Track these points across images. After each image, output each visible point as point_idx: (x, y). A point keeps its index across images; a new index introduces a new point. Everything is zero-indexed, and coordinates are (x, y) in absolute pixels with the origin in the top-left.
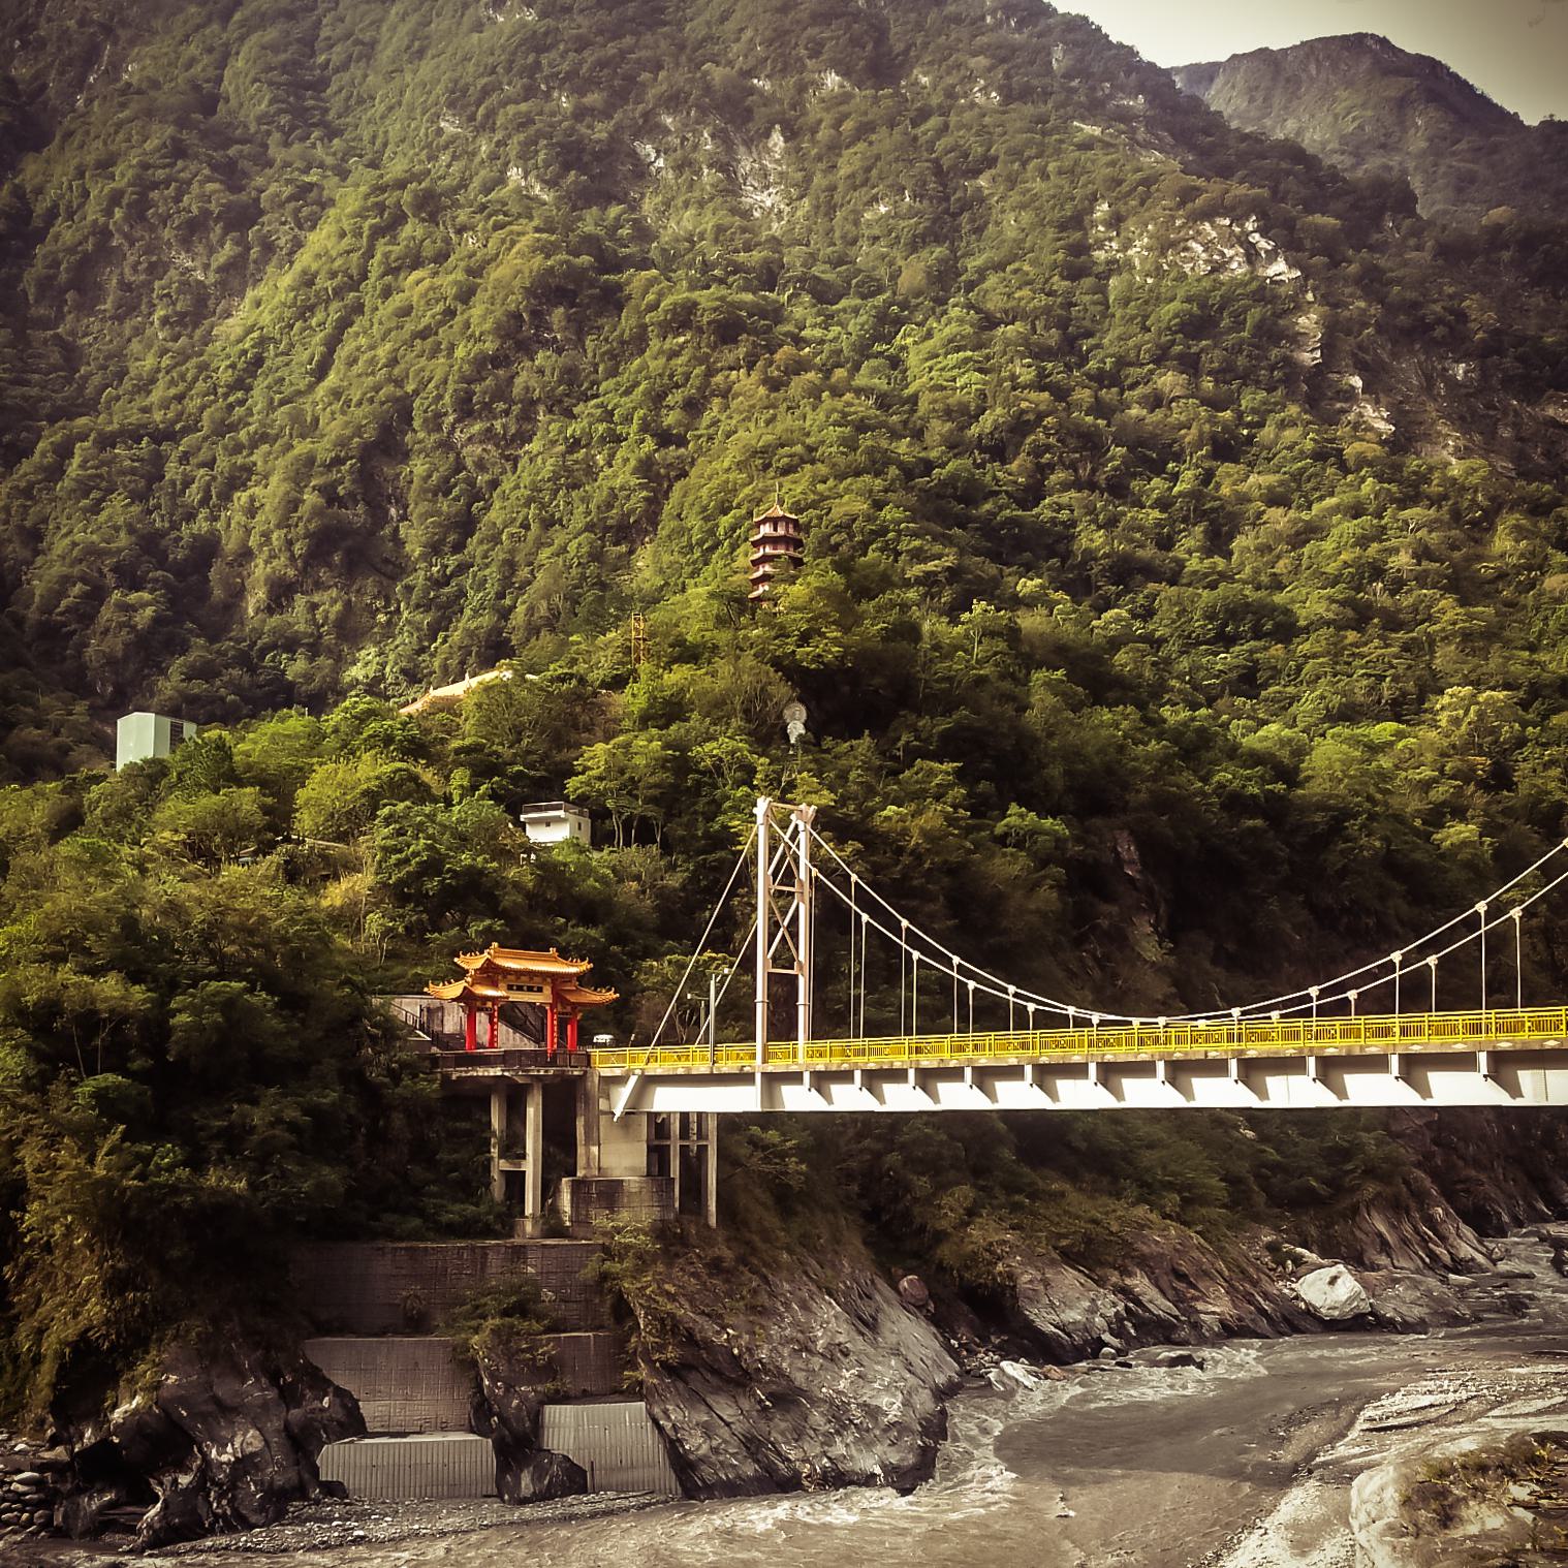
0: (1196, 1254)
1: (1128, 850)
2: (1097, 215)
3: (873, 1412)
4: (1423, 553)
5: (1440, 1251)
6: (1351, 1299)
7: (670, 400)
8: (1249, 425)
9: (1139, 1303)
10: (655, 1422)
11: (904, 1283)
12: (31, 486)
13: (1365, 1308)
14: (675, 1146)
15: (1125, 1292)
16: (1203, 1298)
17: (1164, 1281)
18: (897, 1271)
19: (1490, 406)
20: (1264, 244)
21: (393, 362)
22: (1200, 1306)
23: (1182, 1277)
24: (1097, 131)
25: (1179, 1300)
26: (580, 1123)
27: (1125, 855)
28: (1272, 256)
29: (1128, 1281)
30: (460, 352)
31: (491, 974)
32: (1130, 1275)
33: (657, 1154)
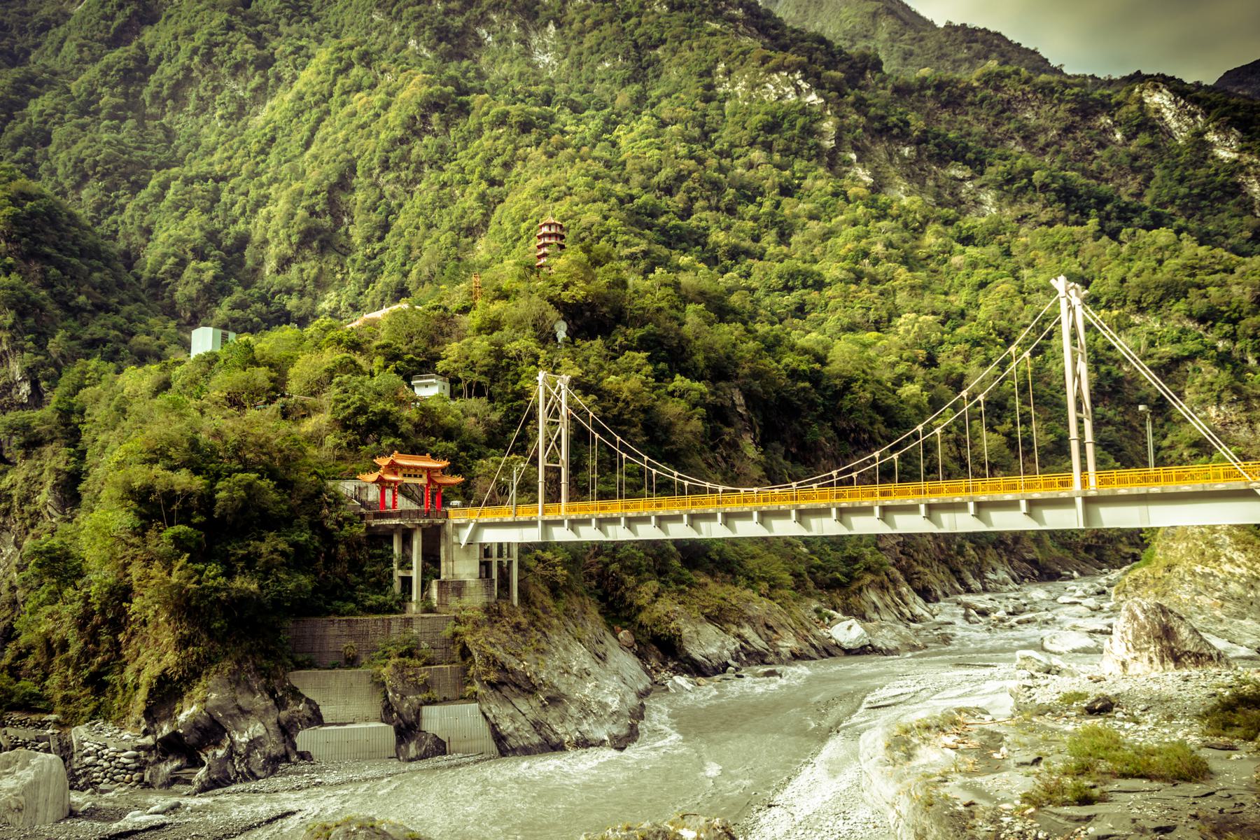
0: (777, 615)
1: (739, 399)
2: (719, 69)
3: (603, 706)
4: (890, 245)
5: (906, 611)
6: (859, 637)
7: (495, 162)
8: (799, 178)
9: (747, 642)
10: (484, 714)
11: (621, 635)
12: (146, 204)
13: (866, 642)
14: (495, 561)
15: (739, 636)
16: (781, 638)
17: (761, 630)
18: (617, 628)
19: (921, 169)
20: (805, 86)
21: (347, 140)
22: (780, 643)
23: (769, 627)
24: (718, 26)
25: (768, 641)
26: (443, 550)
27: (737, 402)
28: (809, 91)
29: (741, 631)
30: (382, 136)
31: (393, 468)
32: (742, 627)
33: (485, 566)
